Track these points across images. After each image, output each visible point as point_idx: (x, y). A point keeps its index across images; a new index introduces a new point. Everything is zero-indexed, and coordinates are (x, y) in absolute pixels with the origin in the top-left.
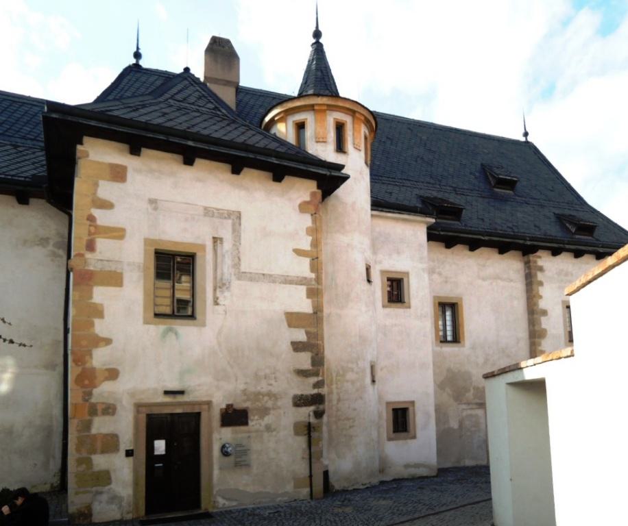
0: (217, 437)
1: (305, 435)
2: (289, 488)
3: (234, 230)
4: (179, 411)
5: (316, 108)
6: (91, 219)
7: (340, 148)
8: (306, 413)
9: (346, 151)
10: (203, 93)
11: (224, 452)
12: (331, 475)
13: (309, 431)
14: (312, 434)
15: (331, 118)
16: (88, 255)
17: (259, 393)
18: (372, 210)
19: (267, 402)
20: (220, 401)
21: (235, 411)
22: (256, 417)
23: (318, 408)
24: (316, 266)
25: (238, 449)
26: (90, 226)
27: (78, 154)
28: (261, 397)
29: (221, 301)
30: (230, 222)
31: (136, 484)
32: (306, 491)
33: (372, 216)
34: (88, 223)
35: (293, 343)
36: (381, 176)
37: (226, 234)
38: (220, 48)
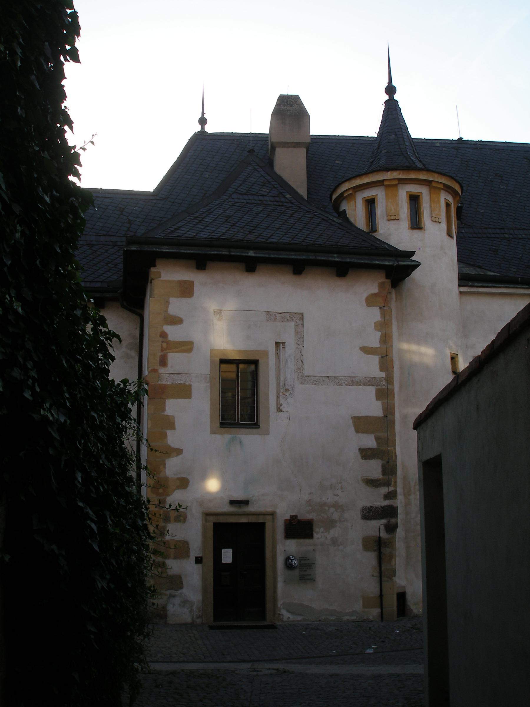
0: (283, 548)
1: (375, 551)
2: (358, 606)
3: (297, 333)
4: (244, 520)
5: (386, 183)
6: (164, 335)
7: (416, 224)
8: (376, 527)
9: (423, 226)
10: (268, 178)
11: (288, 565)
12: (409, 597)
13: (380, 547)
14: (383, 550)
15: (403, 193)
16: (162, 370)
17: (325, 504)
18: (460, 286)
19: (333, 513)
20: (284, 512)
21: (300, 522)
22: (322, 530)
23: (389, 522)
24: (386, 363)
25: (303, 562)
26: (162, 342)
27: (152, 276)
28: (327, 508)
29: (284, 407)
30: (293, 324)
31: (205, 590)
32: (375, 612)
33: (461, 293)
34: (161, 339)
35: (361, 450)
36: (486, 228)
37: (288, 337)
38: (288, 108)
